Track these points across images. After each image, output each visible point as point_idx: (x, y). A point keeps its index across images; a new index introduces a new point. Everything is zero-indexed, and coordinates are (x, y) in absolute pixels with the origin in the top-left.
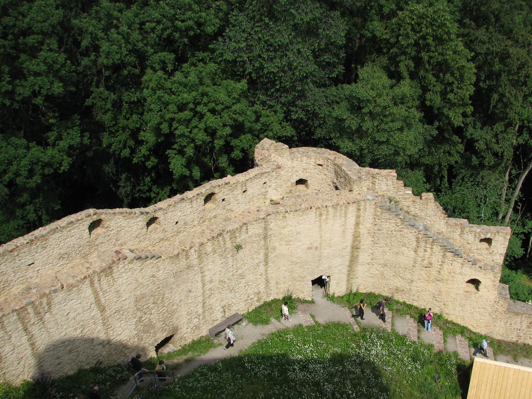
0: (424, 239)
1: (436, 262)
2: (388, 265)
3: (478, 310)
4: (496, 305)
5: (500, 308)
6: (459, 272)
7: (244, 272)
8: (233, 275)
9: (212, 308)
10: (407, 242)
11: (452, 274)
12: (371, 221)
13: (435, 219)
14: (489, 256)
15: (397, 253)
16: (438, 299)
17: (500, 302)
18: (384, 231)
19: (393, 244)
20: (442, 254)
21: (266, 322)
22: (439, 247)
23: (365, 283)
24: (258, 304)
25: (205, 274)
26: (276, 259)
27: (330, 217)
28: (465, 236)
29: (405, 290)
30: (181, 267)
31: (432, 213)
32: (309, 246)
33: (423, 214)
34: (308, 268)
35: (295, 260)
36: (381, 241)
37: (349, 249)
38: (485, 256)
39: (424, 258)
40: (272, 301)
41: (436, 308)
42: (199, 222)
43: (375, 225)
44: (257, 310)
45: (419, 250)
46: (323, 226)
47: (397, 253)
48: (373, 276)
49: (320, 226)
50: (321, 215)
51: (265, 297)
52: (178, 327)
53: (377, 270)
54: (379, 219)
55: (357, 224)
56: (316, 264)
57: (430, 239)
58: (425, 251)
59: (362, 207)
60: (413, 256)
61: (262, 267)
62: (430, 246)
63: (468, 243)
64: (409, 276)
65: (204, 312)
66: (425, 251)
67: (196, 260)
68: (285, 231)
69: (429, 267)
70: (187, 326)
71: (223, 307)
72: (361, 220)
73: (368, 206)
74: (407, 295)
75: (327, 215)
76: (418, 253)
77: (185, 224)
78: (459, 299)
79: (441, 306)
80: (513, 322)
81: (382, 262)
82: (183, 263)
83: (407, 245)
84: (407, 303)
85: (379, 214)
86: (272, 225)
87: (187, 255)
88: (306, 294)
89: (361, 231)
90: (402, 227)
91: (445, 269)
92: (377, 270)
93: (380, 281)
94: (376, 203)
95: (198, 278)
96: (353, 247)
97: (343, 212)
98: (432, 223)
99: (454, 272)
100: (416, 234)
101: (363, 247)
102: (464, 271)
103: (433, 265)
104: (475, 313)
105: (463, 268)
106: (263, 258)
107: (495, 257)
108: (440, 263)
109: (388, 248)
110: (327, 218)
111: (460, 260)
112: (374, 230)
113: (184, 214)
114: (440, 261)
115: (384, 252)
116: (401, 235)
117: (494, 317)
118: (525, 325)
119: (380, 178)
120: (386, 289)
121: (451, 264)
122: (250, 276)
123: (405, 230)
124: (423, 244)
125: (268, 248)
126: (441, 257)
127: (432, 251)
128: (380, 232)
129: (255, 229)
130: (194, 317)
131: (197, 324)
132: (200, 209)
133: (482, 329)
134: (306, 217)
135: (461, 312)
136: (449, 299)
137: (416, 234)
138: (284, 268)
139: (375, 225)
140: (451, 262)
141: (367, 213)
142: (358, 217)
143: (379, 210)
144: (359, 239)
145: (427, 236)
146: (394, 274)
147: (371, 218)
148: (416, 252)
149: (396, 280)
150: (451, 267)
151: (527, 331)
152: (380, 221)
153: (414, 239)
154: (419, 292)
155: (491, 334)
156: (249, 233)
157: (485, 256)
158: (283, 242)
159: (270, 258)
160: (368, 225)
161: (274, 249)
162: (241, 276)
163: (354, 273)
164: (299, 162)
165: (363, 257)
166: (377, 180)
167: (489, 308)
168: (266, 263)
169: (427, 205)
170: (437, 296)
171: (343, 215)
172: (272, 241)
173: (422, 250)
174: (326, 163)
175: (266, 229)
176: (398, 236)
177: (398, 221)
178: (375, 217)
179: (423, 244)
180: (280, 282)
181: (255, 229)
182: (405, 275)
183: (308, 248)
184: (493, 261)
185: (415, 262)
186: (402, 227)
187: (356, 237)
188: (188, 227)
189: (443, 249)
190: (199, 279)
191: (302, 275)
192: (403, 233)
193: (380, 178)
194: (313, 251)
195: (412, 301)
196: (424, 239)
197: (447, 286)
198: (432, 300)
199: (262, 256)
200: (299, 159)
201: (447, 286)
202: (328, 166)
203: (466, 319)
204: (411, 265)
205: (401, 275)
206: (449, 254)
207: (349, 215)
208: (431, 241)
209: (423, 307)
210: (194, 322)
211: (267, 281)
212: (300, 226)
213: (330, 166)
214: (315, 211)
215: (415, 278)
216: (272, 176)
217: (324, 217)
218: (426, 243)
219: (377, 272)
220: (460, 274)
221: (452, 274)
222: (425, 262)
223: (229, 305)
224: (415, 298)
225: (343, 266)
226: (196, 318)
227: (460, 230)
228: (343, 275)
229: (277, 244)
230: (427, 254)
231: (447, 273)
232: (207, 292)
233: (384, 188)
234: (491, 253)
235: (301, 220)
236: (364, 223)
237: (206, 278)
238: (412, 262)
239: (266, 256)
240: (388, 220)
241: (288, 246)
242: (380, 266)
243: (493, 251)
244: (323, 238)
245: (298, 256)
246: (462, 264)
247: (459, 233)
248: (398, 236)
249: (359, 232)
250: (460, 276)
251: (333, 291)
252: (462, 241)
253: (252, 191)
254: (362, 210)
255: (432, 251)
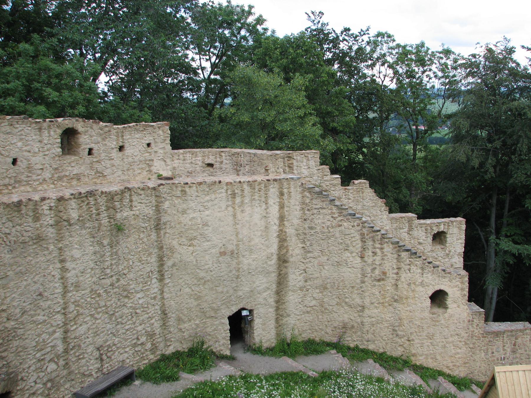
0: (371, 235)
1: (391, 269)
2: (328, 286)
3: (451, 339)
4: (470, 327)
5: (476, 331)
6: (420, 281)
7: (128, 284)
8: (112, 285)
9: (79, 346)
10: (349, 242)
11: (413, 286)
12: (298, 213)
13: (374, 212)
14: (447, 260)
15: (339, 264)
16: (400, 333)
17: (475, 320)
18: (318, 228)
19: (331, 248)
20: (396, 256)
21: (172, 378)
22: (391, 246)
23: (300, 324)
24: (153, 358)
25: (68, 265)
26: (175, 271)
27: (247, 200)
28: (415, 233)
29: (356, 325)
30: (25, 234)
31: (370, 204)
32: (222, 250)
33: (359, 207)
34: (222, 292)
35: (202, 274)
36: (315, 246)
37: (274, 261)
38: (442, 261)
39: (374, 266)
40: (173, 353)
41: (399, 349)
42: (53, 176)
43: (305, 220)
44: (154, 366)
45: (366, 254)
46: (239, 216)
47: (339, 264)
48: (309, 309)
49: (234, 216)
50: (234, 195)
51: (162, 345)
52: (17, 375)
53: (314, 299)
54: (308, 210)
55: (282, 218)
56: (234, 285)
57: (378, 233)
58: (375, 253)
59: (285, 191)
60: (360, 266)
61: (155, 286)
62: (379, 246)
63: (420, 243)
64: (358, 301)
65: (66, 351)
66: (375, 253)
67: (51, 230)
68: (185, 219)
69: (383, 280)
70: (35, 375)
71: (98, 349)
72: (286, 213)
73: (292, 190)
74: (359, 333)
75: (243, 196)
76: (366, 259)
77: (29, 168)
78: (425, 326)
79: (404, 343)
80: (495, 348)
81: (318, 282)
82: (29, 226)
83: (351, 248)
84: (361, 347)
85: (308, 201)
86: (167, 204)
87: (35, 210)
88: (222, 342)
89: (287, 231)
90: (340, 218)
91: (403, 279)
92: (314, 299)
93: (320, 317)
94: (302, 184)
95: (55, 269)
96: (279, 259)
97: (262, 193)
98: (373, 218)
99: (414, 283)
100: (359, 228)
101: (291, 260)
102: (426, 280)
103: (388, 275)
104: (447, 345)
105: (424, 275)
106: (156, 264)
107: (453, 260)
108: (395, 271)
109: (326, 258)
110: (242, 202)
111: (419, 262)
112: (305, 229)
113: (27, 148)
114: (395, 267)
115: (321, 265)
116: (341, 232)
117: (471, 346)
118: (509, 350)
119: (299, 158)
120: (329, 330)
121: (409, 270)
122: (139, 295)
123: (345, 224)
124: (370, 243)
125: (162, 247)
126: (395, 261)
127: (383, 253)
128: (312, 232)
129: (143, 207)
130: (48, 357)
131: (54, 375)
132: (54, 151)
133: (460, 369)
134: (213, 196)
135: (431, 347)
136: (412, 330)
137: (359, 228)
138: (188, 290)
139: (305, 220)
140: (409, 267)
141: (292, 201)
142: (282, 206)
143: (308, 194)
144: (285, 244)
145: (371, 233)
146: (338, 300)
147: (298, 208)
148: (362, 257)
149: (342, 311)
150: (409, 274)
151: (513, 358)
152: (311, 213)
153: (358, 237)
154: (373, 325)
155: (471, 375)
156: (135, 209)
157: (442, 261)
158: (184, 239)
159: (165, 267)
160: (296, 221)
161: (172, 250)
162: (125, 290)
163: (284, 306)
164: (181, 162)
165: (295, 278)
166: (295, 163)
167: (463, 334)
168: (161, 279)
169: (363, 193)
170: (397, 328)
171: (263, 199)
172: (167, 235)
173: (370, 254)
174: (218, 159)
175: (158, 209)
176: (337, 235)
177: (335, 210)
178: (304, 206)
179: (370, 243)
180: (183, 317)
181: (143, 207)
182: (353, 300)
183: (223, 254)
184: (452, 265)
185: (364, 275)
186: (340, 218)
187: (282, 239)
188: (34, 177)
189: (396, 247)
190: (57, 274)
191: (214, 305)
192: (343, 228)
193: (299, 158)
194: (227, 258)
195: (366, 343)
196: (371, 235)
197: (408, 308)
198: (391, 336)
199: (155, 266)
200: (181, 156)
201: (408, 308)
202: (222, 162)
203: (438, 357)
204: (358, 281)
205: (347, 300)
206: (404, 254)
207: (271, 202)
208: (379, 237)
209: (381, 350)
210: (49, 370)
211: (164, 313)
212: (207, 212)
213: (225, 161)
214: (225, 188)
215: (367, 301)
216: (159, 136)
217: (238, 200)
218: (374, 241)
219: (314, 303)
220: (422, 284)
221: (413, 286)
222: (377, 272)
223: (109, 346)
224: (370, 336)
225: (269, 292)
226: (51, 360)
227: (407, 225)
228: (270, 310)
229: (175, 243)
230: (378, 258)
231: (406, 286)
232: (72, 307)
233: (306, 172)
234: (448, 255)
235: (208, 201)
236: (290, 218)
237: (69, 275)
238: (360, 276)
239: (161, 260)
240: (321, 211)
241: (191, 248)
242: (318, 291)
243: (450, 252)
244: (240, 236)
245: (207, 267)
246: (422, 269)
247: (406, 230)
248: (337, 235)
249: (285, 232)
250: (421, 289)
251: (259, 338)
252: (412, 242)
253: (132, 151)
254: (286, 195)
255: (383, 253)
